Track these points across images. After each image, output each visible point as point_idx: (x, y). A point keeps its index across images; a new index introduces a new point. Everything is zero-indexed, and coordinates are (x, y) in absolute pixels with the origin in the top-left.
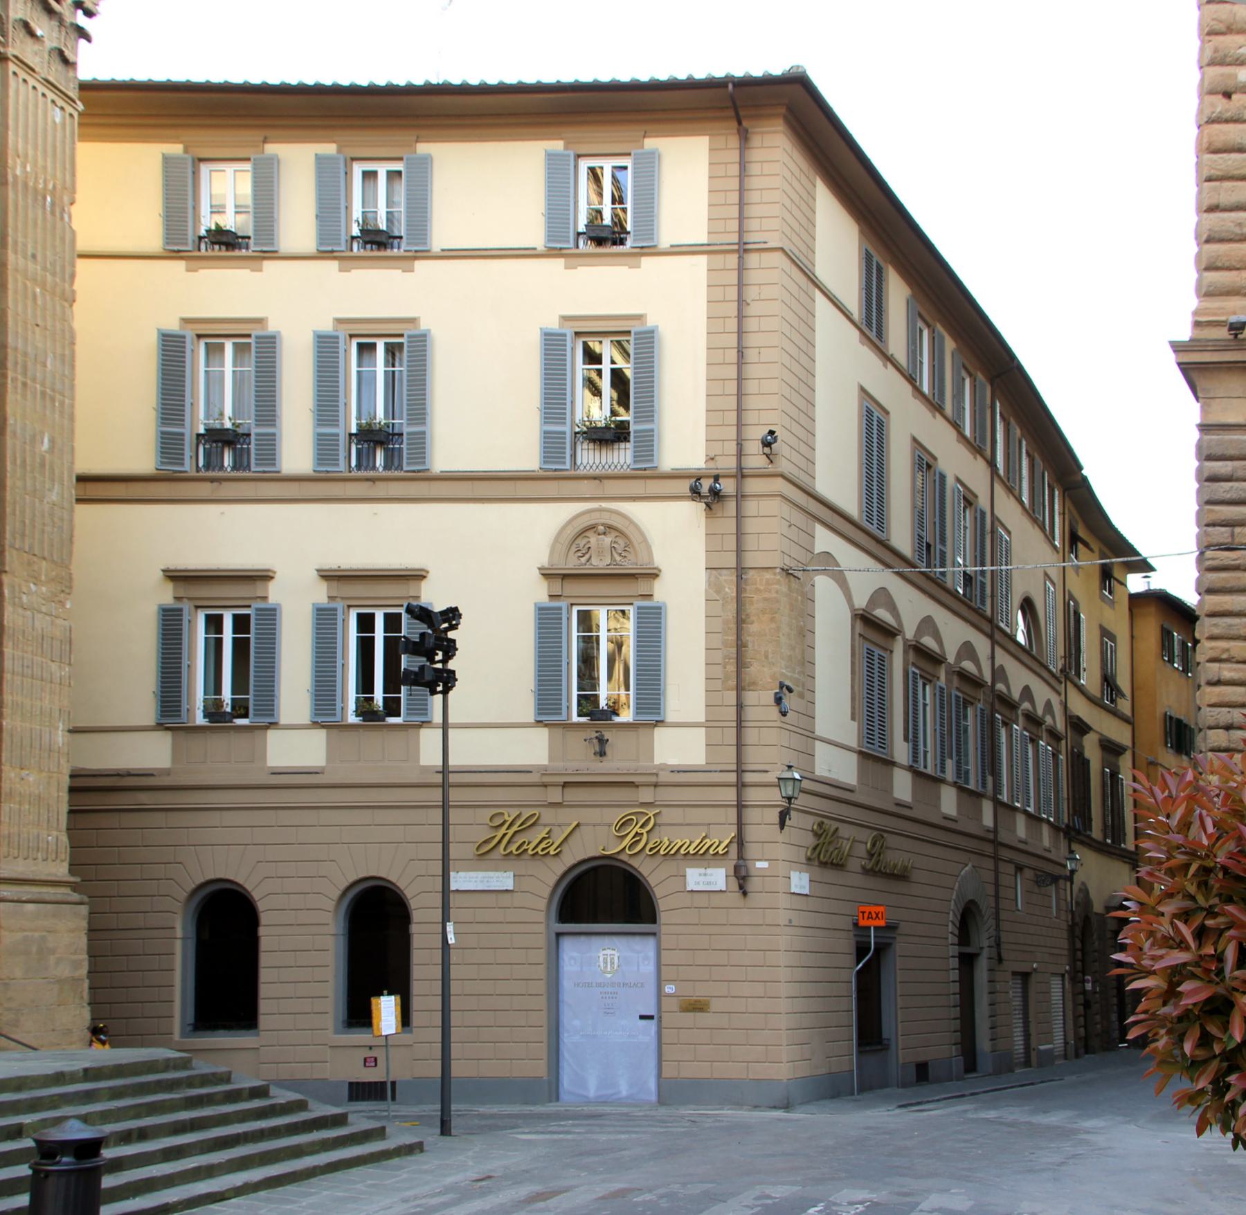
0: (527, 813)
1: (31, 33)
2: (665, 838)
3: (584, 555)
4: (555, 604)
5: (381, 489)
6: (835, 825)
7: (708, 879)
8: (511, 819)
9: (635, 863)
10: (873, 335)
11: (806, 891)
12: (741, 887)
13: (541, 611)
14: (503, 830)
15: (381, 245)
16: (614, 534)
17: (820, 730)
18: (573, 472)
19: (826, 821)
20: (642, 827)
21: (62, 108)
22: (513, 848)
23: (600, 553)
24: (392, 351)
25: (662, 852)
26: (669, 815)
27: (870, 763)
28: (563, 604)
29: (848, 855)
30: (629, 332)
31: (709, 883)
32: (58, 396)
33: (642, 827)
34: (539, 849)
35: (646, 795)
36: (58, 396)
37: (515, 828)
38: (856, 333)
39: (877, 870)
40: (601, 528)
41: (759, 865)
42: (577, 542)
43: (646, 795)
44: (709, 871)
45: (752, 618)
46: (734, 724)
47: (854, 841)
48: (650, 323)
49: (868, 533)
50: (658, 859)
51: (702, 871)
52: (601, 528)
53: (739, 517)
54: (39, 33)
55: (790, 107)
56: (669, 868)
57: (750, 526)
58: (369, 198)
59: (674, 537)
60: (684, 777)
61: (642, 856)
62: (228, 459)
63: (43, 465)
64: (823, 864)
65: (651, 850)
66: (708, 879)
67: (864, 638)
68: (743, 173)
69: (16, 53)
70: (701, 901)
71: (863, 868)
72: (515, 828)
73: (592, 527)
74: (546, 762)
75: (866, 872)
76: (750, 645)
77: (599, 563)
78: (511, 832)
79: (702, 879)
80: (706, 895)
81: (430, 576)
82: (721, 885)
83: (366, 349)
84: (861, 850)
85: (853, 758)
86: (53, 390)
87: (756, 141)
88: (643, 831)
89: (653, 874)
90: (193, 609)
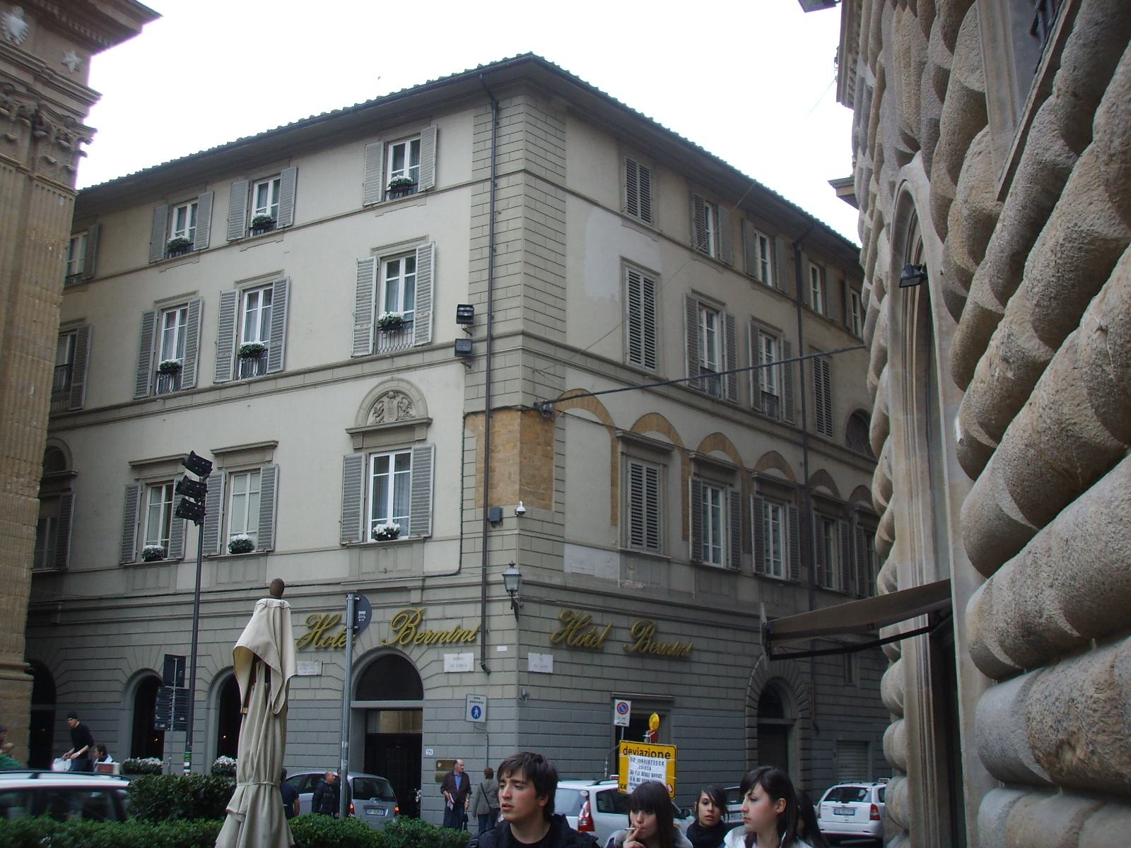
0: (332, 614)
1: (49, 163)
2: (432, 627)
3: (379, 415)
4: (358, 454)
5: (256, 388)
6: (586, 614)
7: (460, 662)
8: (320, 621)
9: (407, 652)
10: (638, 219)
11: (550, 670)
12: (483, 667)
13: (346, 460)
14: (315, 630)
15: (405, 192)
16: (401, 396)
17: (570, 532)
18: (374, 356)
19: (575, 611)
20: (412, 622)
21: (65, 197)
22: (322, 642)
23: (390, 414)
24: (268, 295)
25: (426, 642)
26: (432, 612)
27: (632, 562)
28: (362, 454)
29: (605, 640)
30: (271, 284)
31: (461, 665)
32: (42, 361)
33: (412, 622)
34: (339, 643)
35: (415, 597)
36: (42, 361)
37: (323, 627)
38: (618, 221)
39: (643, 651)
40: (391, 393)
41: (500, 649)
42: (375, 406)
43: (415, 597)
44: (461, 655)
45: (500, 448)
46: (482, 535)
47: (612, 627)
48: (286, 276)
49: (637, 370)
50: (424, 647)
51: (456, 655)
52: (391, 393)
53: (489, 371)
54: (53, 160)
55: (525, 88)
56: (432, 654)
57: (498, 375)
58: (180, 225)
59: (443, 393)
60: (450, 580)
61: (412, 647)
62: (255, 369)
63: (27, 403)
64: (573, 648)
65: (418, 640)
66: (460, 662)
67: (627, 455)
68: (495, 137)
69: (39, 175)
70: (455, 680)
71: (626, 649)
72: (323, 627)
73: (386, 394)
74: (346, 576)
75: (629, 654)
76: (497, 470)
77: (389, 420)
78: (320, 630)
79: (455, 662)
80: (459, 675)
81: (280, 446)
82: (470, 667)
83: (393, 269)
84: (624, 635)
85: (617, 558)
86: (39, 357)
87: (504, 113)
88: (412, 625)
89: (421, 659)
90: (144, 487)
